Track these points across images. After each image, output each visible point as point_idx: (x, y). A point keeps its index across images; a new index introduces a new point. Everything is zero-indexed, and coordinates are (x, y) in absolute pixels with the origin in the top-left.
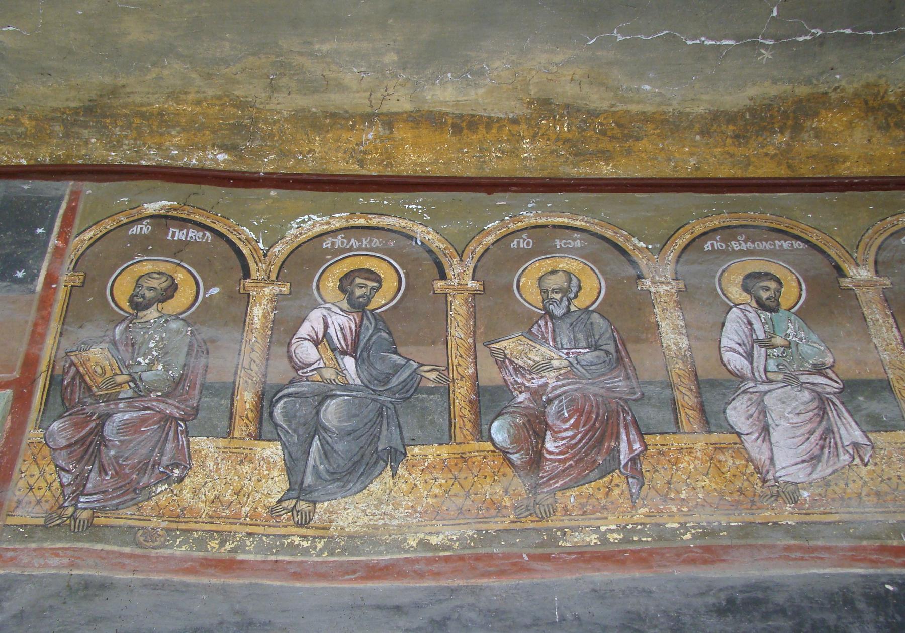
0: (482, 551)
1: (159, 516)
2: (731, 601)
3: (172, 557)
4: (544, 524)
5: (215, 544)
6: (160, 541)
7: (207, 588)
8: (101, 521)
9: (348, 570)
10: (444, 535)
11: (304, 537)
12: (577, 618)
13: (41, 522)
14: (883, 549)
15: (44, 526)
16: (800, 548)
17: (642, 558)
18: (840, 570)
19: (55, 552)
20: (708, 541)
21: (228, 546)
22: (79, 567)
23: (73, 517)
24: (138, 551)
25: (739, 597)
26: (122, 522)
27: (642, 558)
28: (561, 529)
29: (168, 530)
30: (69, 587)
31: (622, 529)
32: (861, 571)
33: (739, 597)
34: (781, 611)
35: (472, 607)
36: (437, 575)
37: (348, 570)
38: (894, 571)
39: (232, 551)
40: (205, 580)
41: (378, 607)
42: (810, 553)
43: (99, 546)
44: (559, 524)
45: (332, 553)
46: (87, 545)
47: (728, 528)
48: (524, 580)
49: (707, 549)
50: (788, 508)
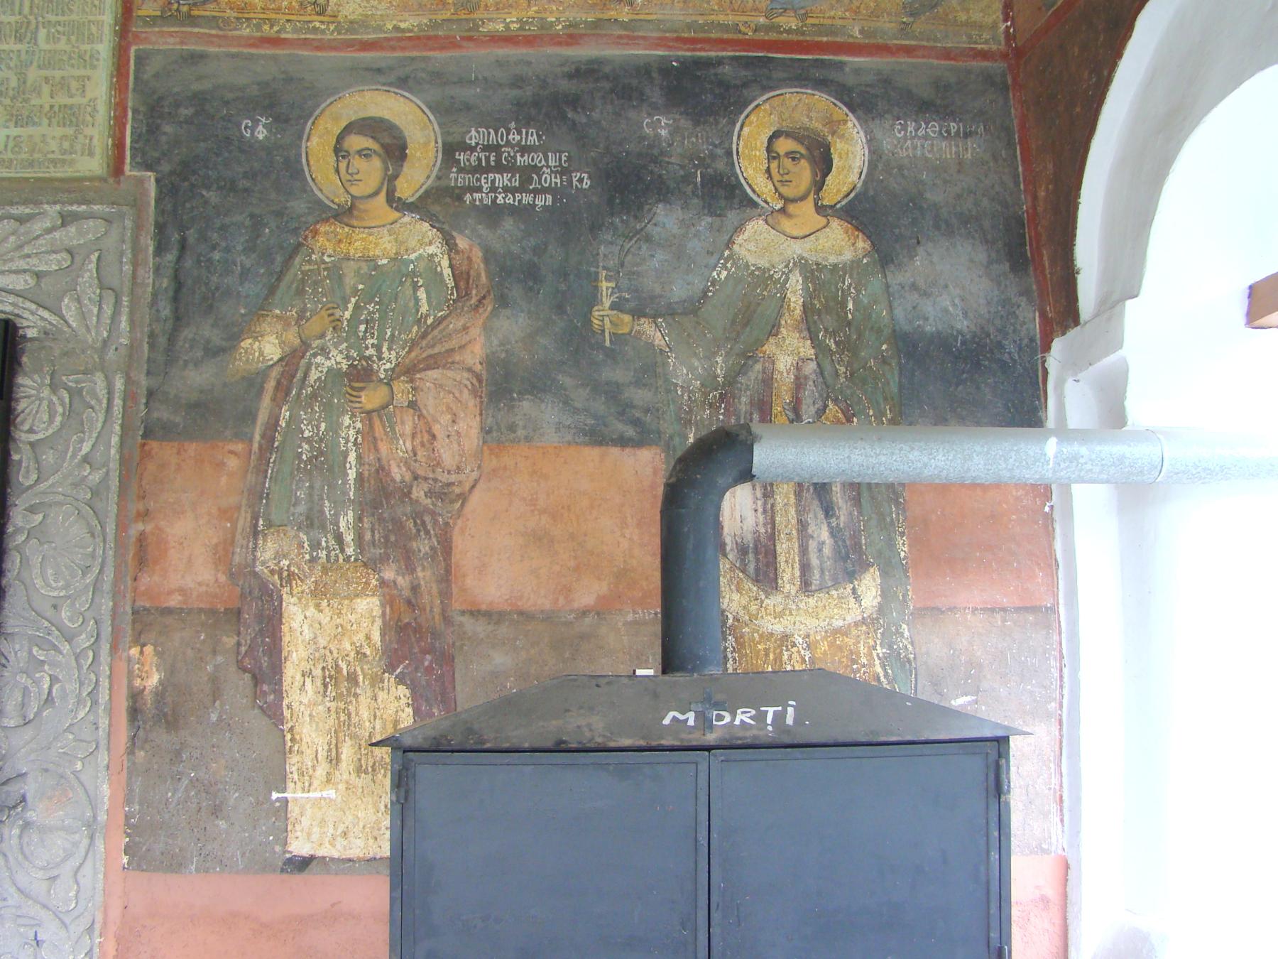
0: (432, 33)
1: (231, 9)
2: (577, 70)
3: (240, 37)
4: (472, 16)
5: (266, 27)
6: (233, 26)
7: (263, 57)
8: (195, 13)
9: (349, 45)
10: (409, 22)
11: (322, 22)
12: (485, 79)
13: (159, 13)
14: (678, 39)
15: (161, 16)
16: (628, 37)
17: (530, 41)
18: (647, 52)
19: (171, 34)
20: (571, 31)
21: (276, 28)
22: (186, 44)
23: (178, 10)
24: (221, 33)
25: (583, 67)
26: (208, 13)
27: (530, 41)
28: (482, 20)
29: (238, 19)
30: (182, 57)
31: (520, 21)
32: (660, 53)
33: (583, 67)
34: (607, 77)
35: (423, 70)
36: (403, 49)
37: (349, 45)
38: (680, 53)
39: (279, 32)
40: (262, 52)
41: (367, 69)
42: (632, 40)
43: (196, 30)
44: (481, 16)
45: (339, 33)
46: (189, 29)
47: (586, 22)
48: (456, 53)
49: (571, 36)
50: (626, 9)
